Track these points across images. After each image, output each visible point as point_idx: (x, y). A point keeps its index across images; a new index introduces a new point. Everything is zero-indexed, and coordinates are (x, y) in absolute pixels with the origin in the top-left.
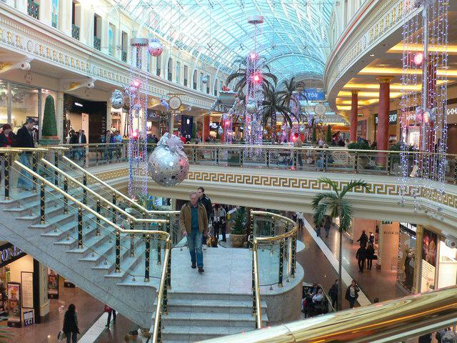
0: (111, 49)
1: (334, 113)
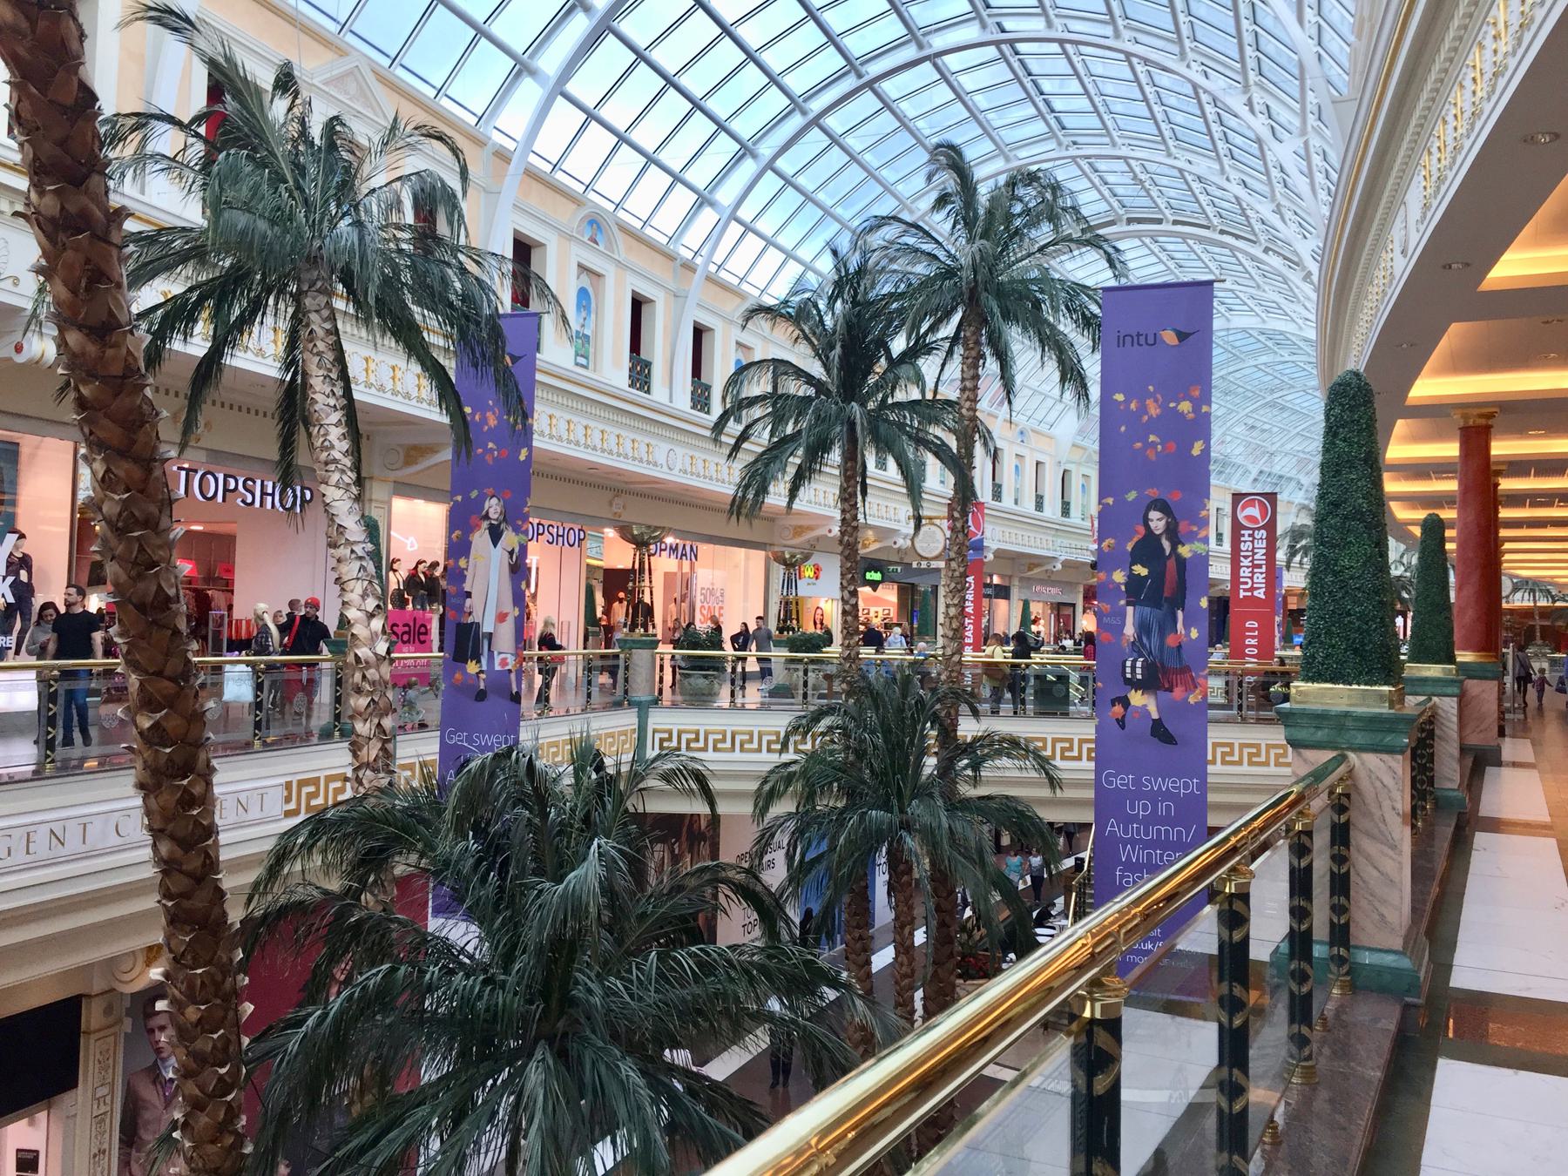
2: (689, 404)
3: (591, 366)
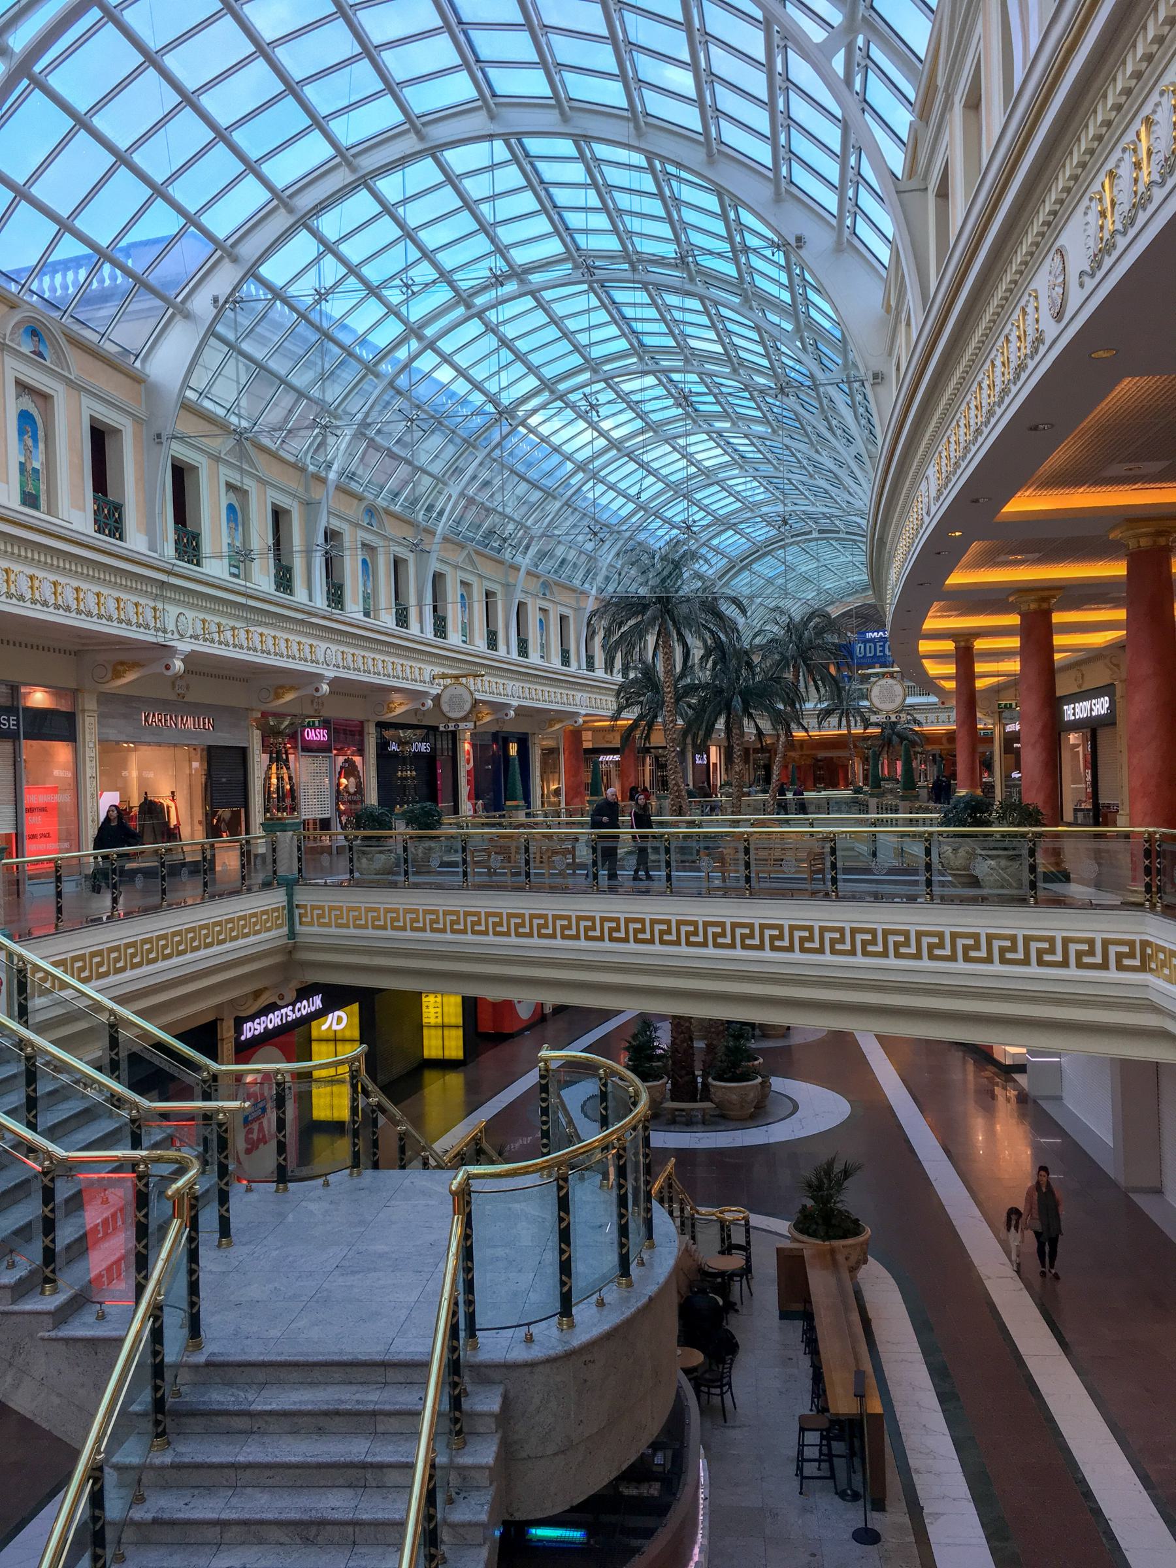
0: (241, 558)
1: (933, 699)
2: (273, 587)
3: (242, 576)
